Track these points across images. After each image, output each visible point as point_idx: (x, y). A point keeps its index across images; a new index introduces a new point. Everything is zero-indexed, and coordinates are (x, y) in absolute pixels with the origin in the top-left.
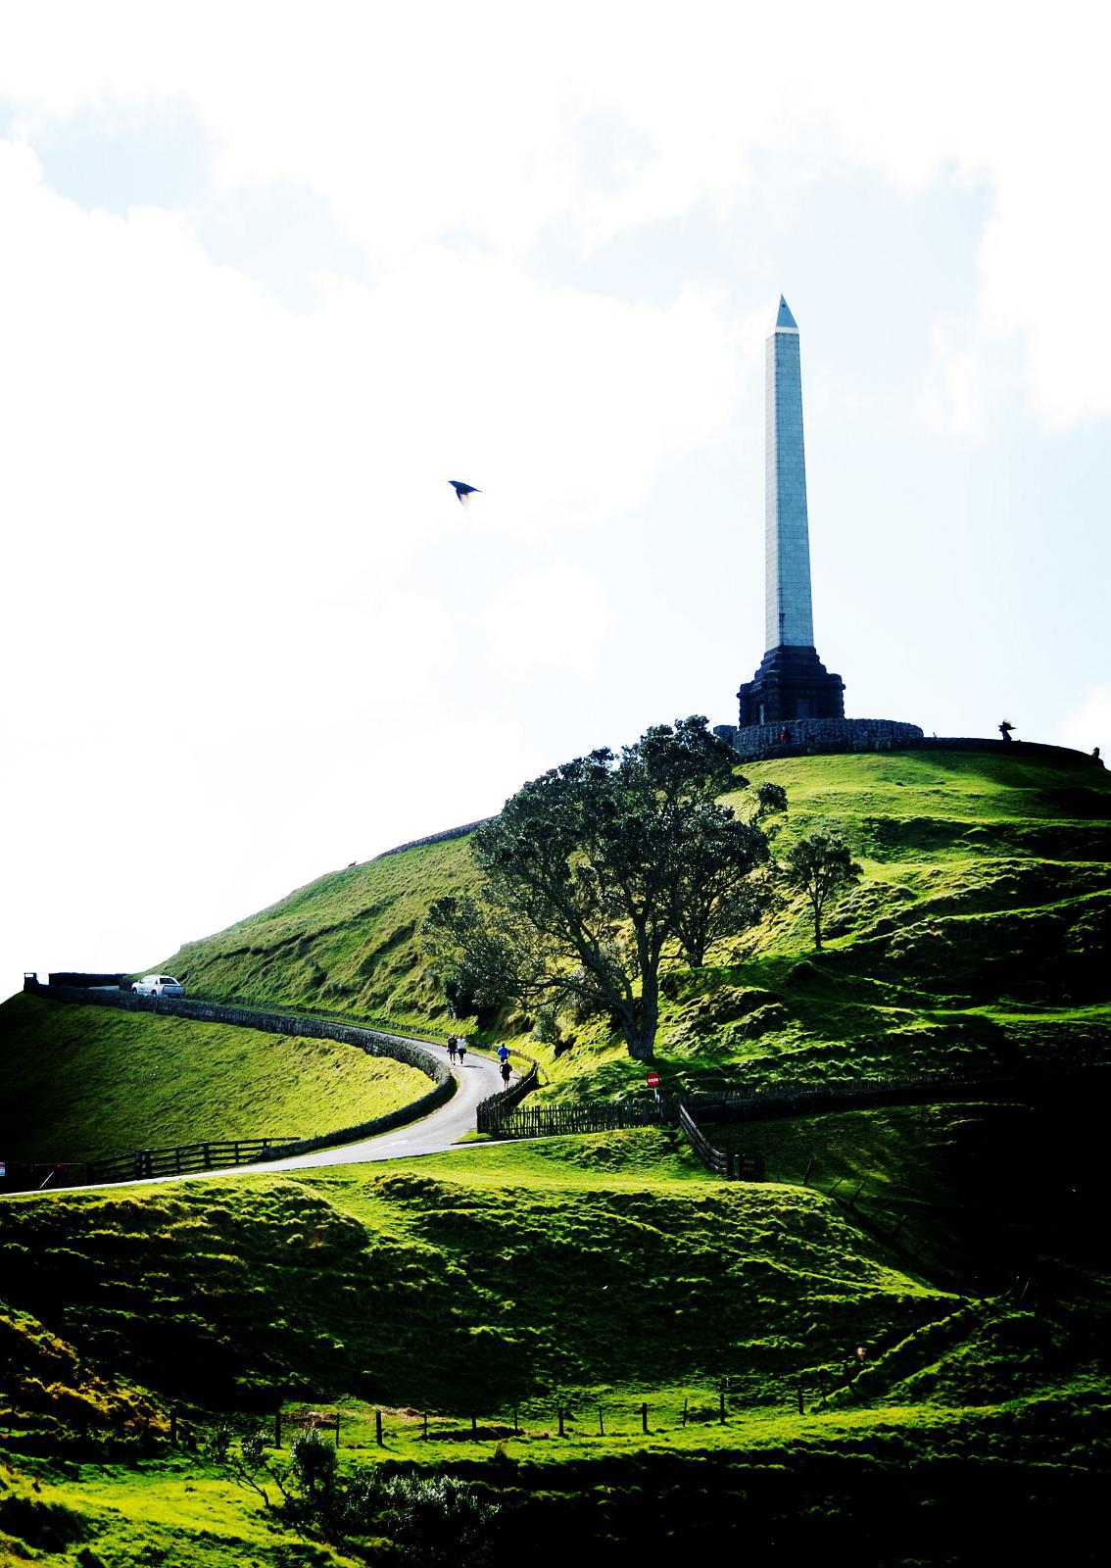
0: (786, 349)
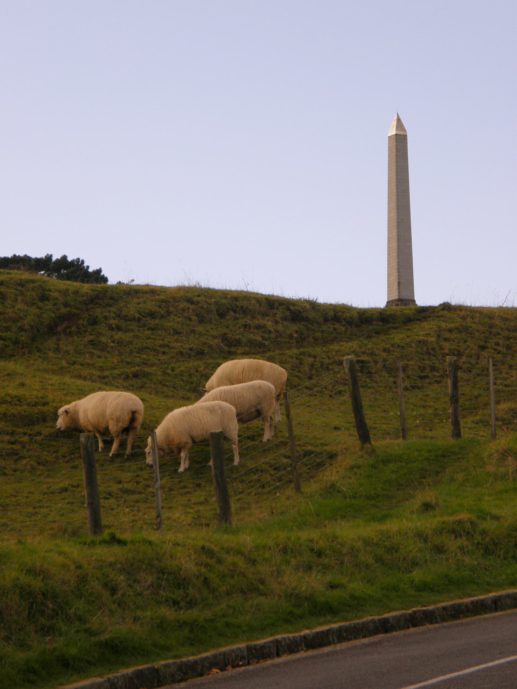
0: (399, 144)
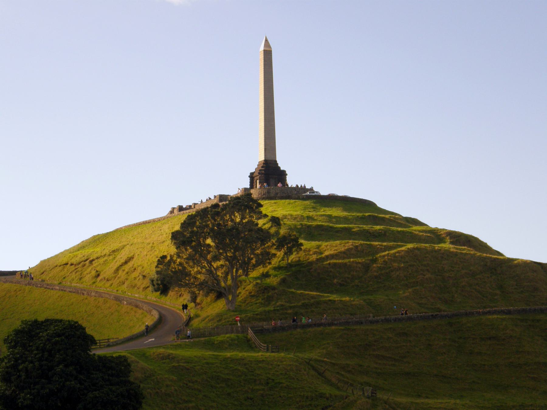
0: (268, 54)
